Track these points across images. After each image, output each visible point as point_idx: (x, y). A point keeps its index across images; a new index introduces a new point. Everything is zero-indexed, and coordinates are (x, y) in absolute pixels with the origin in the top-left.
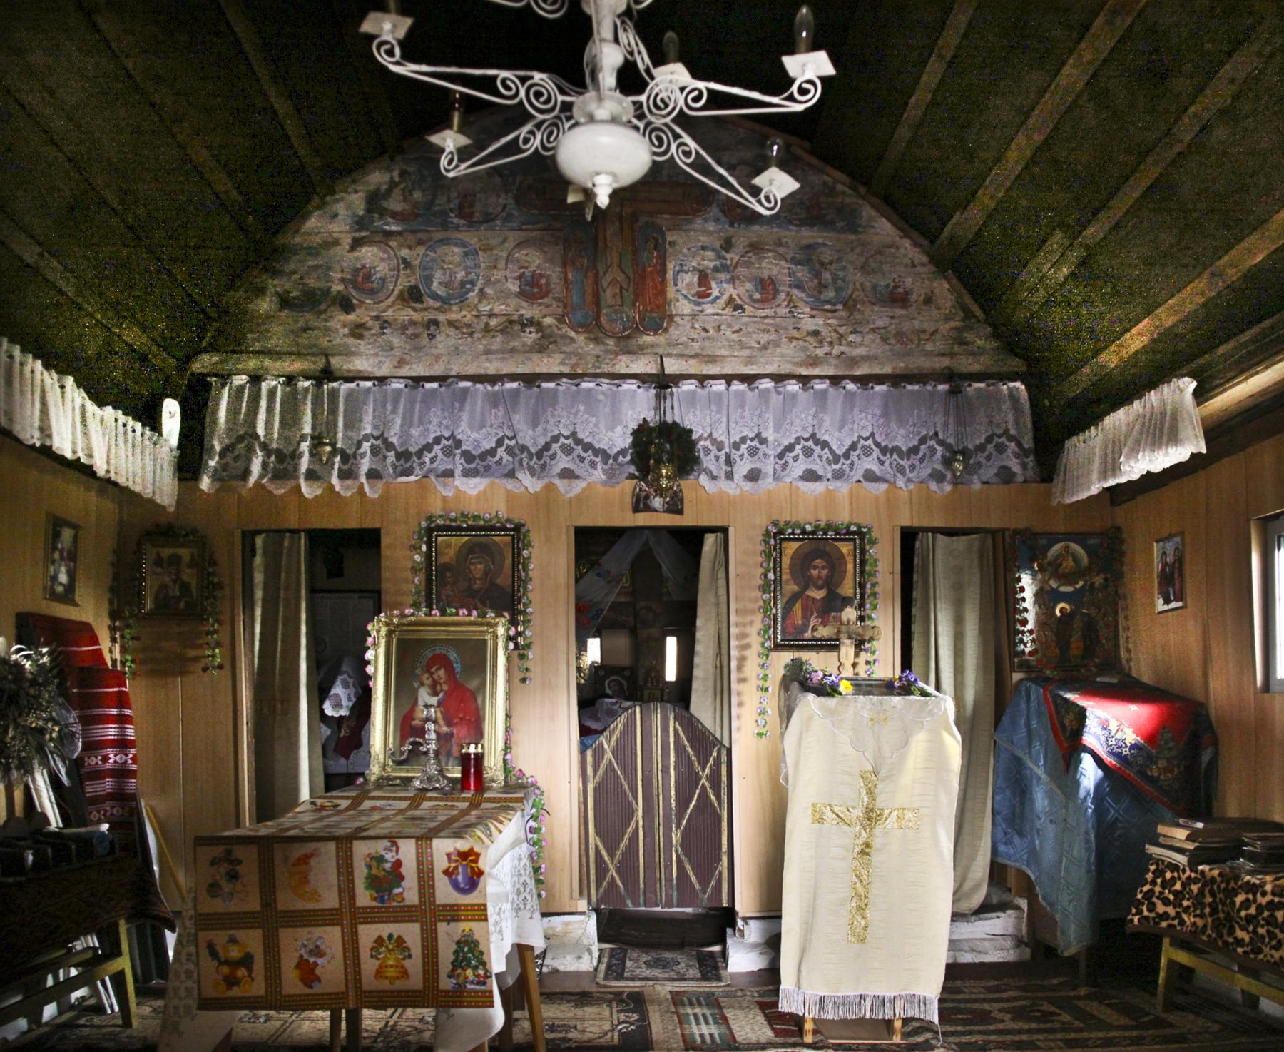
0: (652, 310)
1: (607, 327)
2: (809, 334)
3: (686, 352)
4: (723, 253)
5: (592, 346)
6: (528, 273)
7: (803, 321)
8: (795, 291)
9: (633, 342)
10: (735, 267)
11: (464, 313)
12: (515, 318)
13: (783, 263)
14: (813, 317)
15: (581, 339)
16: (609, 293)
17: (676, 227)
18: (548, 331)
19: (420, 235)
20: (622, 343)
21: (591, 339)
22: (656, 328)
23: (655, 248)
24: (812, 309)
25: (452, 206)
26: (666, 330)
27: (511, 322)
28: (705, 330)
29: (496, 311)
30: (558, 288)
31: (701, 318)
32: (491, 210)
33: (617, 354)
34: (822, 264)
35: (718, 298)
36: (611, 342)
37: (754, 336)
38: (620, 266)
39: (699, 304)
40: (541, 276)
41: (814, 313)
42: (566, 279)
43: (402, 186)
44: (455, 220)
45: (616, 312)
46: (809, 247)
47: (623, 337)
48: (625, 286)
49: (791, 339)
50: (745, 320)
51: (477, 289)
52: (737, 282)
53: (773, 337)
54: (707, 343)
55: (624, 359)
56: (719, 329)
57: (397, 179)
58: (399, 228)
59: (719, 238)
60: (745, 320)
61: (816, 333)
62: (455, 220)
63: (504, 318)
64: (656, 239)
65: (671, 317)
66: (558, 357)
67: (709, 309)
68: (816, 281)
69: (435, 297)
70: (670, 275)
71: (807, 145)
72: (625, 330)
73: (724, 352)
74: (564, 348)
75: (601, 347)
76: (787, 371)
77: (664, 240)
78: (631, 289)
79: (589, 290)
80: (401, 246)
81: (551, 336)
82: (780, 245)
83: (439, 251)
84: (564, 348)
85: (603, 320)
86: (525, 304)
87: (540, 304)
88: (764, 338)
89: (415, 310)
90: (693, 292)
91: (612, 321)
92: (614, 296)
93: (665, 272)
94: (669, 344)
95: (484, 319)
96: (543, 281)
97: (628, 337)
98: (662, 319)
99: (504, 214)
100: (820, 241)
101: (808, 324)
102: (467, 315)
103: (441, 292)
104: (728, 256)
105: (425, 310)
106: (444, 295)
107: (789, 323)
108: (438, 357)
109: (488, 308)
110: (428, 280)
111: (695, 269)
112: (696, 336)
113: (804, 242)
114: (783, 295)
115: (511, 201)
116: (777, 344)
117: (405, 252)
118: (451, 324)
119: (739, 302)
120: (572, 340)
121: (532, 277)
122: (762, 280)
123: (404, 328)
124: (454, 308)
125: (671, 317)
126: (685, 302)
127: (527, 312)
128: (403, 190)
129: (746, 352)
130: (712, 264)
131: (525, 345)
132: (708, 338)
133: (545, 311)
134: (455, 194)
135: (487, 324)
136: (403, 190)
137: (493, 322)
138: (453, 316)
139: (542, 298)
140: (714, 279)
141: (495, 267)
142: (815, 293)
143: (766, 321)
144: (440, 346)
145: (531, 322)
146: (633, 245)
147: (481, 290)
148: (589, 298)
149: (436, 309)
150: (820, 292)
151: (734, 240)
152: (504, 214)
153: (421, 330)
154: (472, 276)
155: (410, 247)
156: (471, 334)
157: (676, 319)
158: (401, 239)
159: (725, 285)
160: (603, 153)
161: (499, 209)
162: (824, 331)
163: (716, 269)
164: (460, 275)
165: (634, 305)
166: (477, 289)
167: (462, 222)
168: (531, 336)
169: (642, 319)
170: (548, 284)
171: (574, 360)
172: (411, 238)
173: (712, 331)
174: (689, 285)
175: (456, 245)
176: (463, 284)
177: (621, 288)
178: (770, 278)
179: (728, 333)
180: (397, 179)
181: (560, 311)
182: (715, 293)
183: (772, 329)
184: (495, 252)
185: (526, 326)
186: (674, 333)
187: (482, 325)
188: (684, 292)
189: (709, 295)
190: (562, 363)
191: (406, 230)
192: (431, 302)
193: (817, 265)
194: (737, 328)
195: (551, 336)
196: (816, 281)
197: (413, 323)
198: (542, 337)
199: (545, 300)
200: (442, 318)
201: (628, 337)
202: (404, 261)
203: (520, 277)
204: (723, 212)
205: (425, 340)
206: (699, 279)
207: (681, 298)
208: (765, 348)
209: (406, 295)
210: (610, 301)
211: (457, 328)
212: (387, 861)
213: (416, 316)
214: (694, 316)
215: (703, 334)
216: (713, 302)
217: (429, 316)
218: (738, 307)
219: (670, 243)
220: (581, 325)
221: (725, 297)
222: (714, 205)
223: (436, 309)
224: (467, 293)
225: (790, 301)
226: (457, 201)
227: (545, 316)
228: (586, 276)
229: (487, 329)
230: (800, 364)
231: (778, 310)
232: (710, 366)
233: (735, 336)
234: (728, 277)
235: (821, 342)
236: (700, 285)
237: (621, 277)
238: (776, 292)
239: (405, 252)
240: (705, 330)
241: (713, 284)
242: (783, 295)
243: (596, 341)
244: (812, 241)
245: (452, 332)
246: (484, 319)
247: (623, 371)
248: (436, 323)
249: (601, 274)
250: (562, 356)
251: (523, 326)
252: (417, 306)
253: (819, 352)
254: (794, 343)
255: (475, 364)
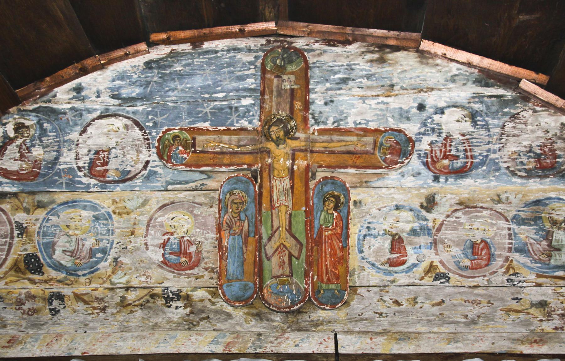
0: (329, 281)
1: (272, 300)
2: (532, 305)
3: (371, 329)
4: (424, 213)
5: (253, 322)
6: (174, 240)
7: (526, 291)
8: (516, 256)
9: (306, 317)
10: (439, 230)
11: (93, 286)
12: (158, 291)
13: (502, 223)
14: (539, 285)
15: (239, 314)
16: (275, 260)
17: (364, 184)
18: (200, 305)
19: (39, 197)
20: (171, 320)
21: (253, 315)
22: (335, 301)
23: (336, 208)
24: (538, 276)
25: (81, 164)
26: (347, 304)
27: (153, 296)
28: (397, 303)
29: (134, 283)
30: (212, 257)
31: (391, 289)
32: (129, 168)
33: (284, 331)
34: (554, 223)
35: (415, 265)
36: (277, 318)
37: (460, 309)
38: (289, 231)
39: (390, 273)
40: (190, 243)
41: (540, 280)
42: (220, 247)
43: (19, 141)
44: (85, 180)
45: (283, 283)
46: (537, 202)
47: (292, 312)
48: (295, 253)
49: (509, 311)
50: (449, 290)
51: (110, 259)
52: (440, 247)
53: (486, 309)
54: (397, 318)
55: (293, 336)
56: (414, 301)
57: (12, 134)
58: (14, 190)
59: (418, 196)
60: (449, 290)
61: (543, 304)
62: (85, 180)
63: (146, 292)
64: (337, 198)
65: (354, 289)
66: (210, 335)
67: (403, 279)
68: (545, 243)
69: (59, 267)
70: (353, 240)
71: (543, 78)
72: (293, 303)
73: (420, 328)
74: (218, 325)
75: (265, 324)
76: (504, 350)
77: (348, 199)
78: (303, 256)
79: (250, 258)
80: (17, 209)
81: (202, 311)
82: (499, 201)
83: (62, 215)
84: (218, 325)
85: (266, 293)
86: (170, 276)
87: (189, 276)
88: (473, 311)
89: (33, 282)
90: (383, 260)
91: (279, 294)
92: (281, 265)
93: (348, 236)
94: (350, 320)
95: (121, 292)
96: (193, 249)
97: (299, 311)
98: (342, 291)
99: (145, 172)
100: (553, 195)
101: (533, 294)
102: (96, 288)
103: (66, 261)
104: (429, 216)
105: (46, 282)
106: (69, 265)
107: (507, 294)
108: (58, 336)
109: (124, 280)
110: (50, 247)
111: (386, 232)
112: (384, 310)
113: (532, 198)
114: (500, 261)
115: (154, 157)
116: (488, 318)
117: (20, 217)
118: (78, 297)
119: (442, 269)
120: (229, 316)
121: (180, 244)
122: (473, 245)
123: (20, 303)
124: (82, 280)
125: (354, 289)
126: (373, 271)
127: (174, 282)
128: (20, 147)
129: (450, 328)
130: (408, 227)
131: (170, 321)
132: (401, 312)
133: (194, 283)
134: (85, 151)
135: (123, 298)
136: (20, 147)
137: (131, 296)
138: (82, 290)
139: (190, 269)
140: (410, 244)
141: (133, 233)
142: (543, 257)
143: (476, 291)
144: (65, 323)
145: (178, 296)
146: (307, 204)
147: (115, 260)
148: (249, 268)
149: (59, 281)
150: (550, 256)
151: (438, 198)
152: (145, 172)
153: (41, 304)
154: (104, 244)
155: (27, 211)
156: (104, 309)
157: (359, 291)
158: (15, 201)
159: (424, 251)
160: (278, 62)
161: (140, 166)
162: (554, 303)
163: (414, 232)
164: (90, 242)
165: (306, 275)
166: (110, 259)
167: (93, 181)
168: (177, 311)
169: (316, 291)
170: (199, 252)
171: (229, 338)
172: (27, 200)
173: (405, 304)
174: (378, 252)
175: (85, 208)
176: (92, 253)
177: (290, 255)
178: (483, 241)
179: (427, 306)
180: (12, 134)
181: (214, 282)
182: (411, 259)
183: (484, 301)
184: (133, 216)
185: (172, 299)
186: (356, 306)
187: (118, 300)
188: (372, 259)
189: (403, 263)
190: (214, 341)
191: (23, 192)
192: (53, 273)
193: (548, 226)
194: (438, 300)
195: (202, 311)
196: (545, 243)
197: (31, 297)
198: (191, 312)
199: (196, 271)
200: (67, 291)
201: (299, 311)
202: (19, 226)
203: (164, 245)
204: (426, 164)
205: (46, 315)
206: (392, 243)
207: (367, 266)
208: (474, 322)
209: (22, 266)
210: (277, 271)
211: (86, 302)
212: (302, 158)
213: (35, 289)
214: (383, 287)
215: (395, 308)
216: (410, 269)
217: (50, 289)
218: (440, 276)
219: (355, 202)
220: (238, 299)
221: (425, 265)
222: (414, 156)
223: (59, 281)
224: (97, 263)
225: (508, 269)
226: (87, 159)
227: (195, 289)
228: (245, 242)
229: (123, 304)
230: (521, 341)
231: (493, 278)
232: (403, 344)
233: (436, 310)
234: (430, 240)
235: (549, 315)
236: (392, 250)
237: (290, 242)
238: (491, 257)
239: (20, 217)
240: (397, 303)
241: (409, 250)
242: (500, 261)
243: (259, 316)
244: (540, 196)
245: (81, 306)
246: (121, 292)
247: (290, 351)
248: (60, 297)
249: (265, 239)
250: (215, 334)
251: (168, 300)
252: (36, 277)
253: (548, 327)
254: (513, 316)
255: (106, 343)
